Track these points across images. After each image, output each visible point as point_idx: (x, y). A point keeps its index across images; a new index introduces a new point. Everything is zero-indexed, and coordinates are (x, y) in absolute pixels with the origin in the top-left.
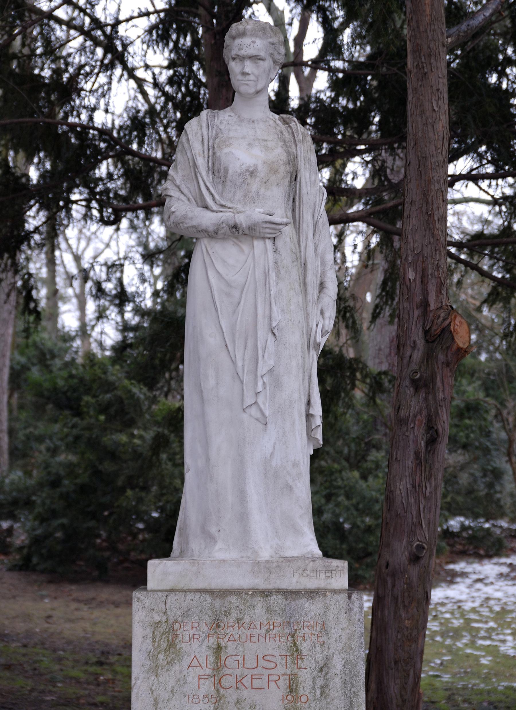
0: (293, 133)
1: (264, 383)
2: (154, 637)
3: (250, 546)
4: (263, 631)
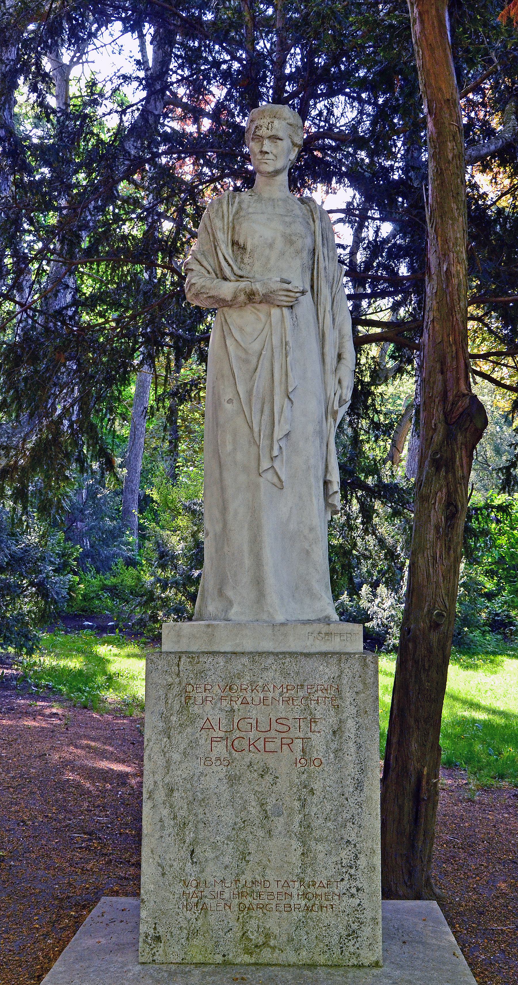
0: (311, 211)
1: (280, 448)
2: (167, 698)
3: (265, 609)
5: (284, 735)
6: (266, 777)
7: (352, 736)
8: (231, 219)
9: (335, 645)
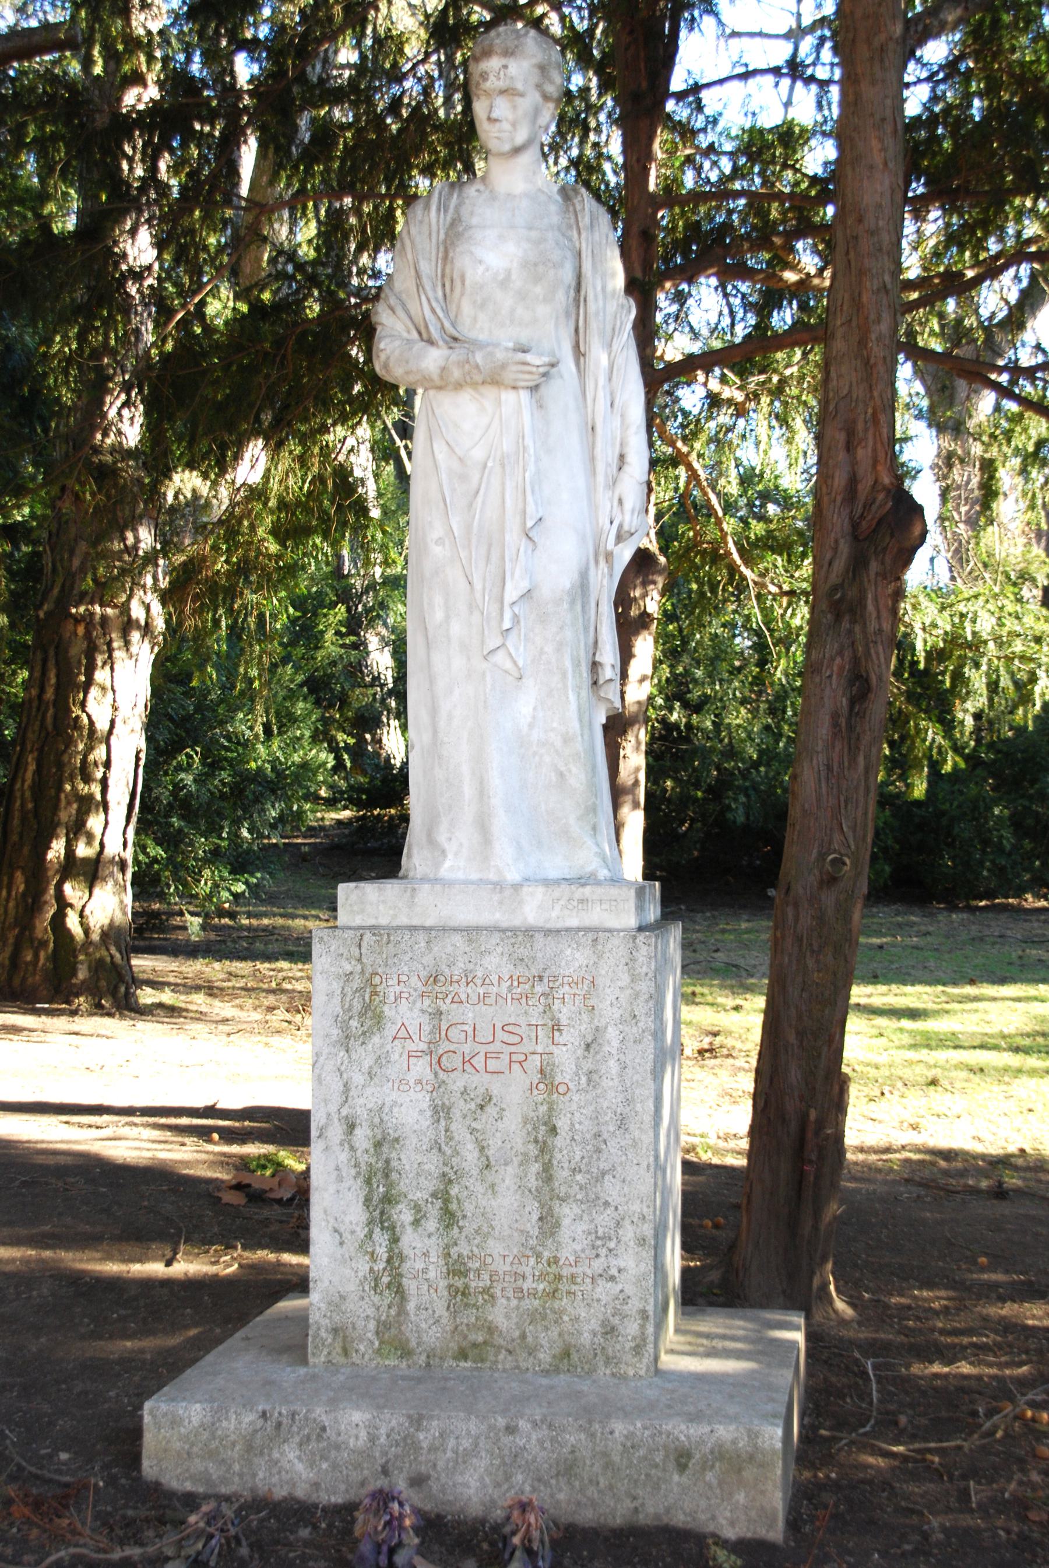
4: (504, 989)
5: (513, 1049)
6: (488, 1109)
7: (614, 1052)
8: (442, 236)
9: (596, 916)
